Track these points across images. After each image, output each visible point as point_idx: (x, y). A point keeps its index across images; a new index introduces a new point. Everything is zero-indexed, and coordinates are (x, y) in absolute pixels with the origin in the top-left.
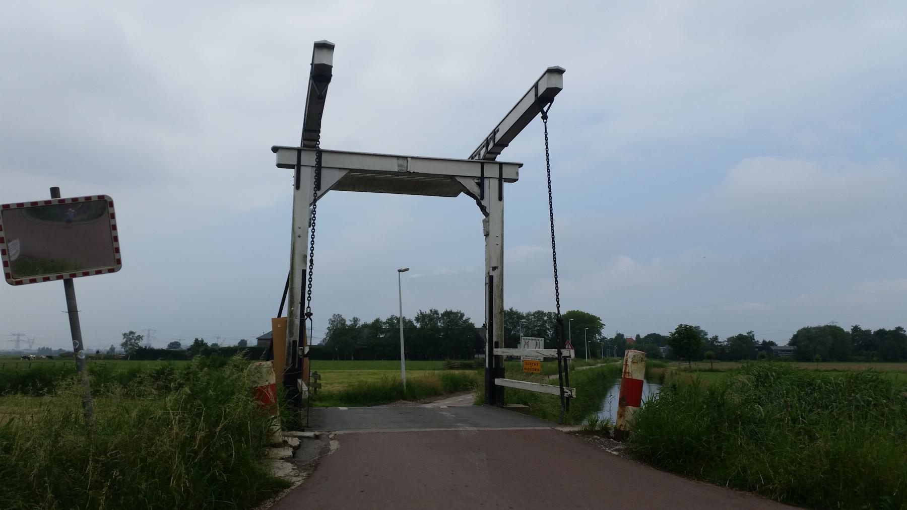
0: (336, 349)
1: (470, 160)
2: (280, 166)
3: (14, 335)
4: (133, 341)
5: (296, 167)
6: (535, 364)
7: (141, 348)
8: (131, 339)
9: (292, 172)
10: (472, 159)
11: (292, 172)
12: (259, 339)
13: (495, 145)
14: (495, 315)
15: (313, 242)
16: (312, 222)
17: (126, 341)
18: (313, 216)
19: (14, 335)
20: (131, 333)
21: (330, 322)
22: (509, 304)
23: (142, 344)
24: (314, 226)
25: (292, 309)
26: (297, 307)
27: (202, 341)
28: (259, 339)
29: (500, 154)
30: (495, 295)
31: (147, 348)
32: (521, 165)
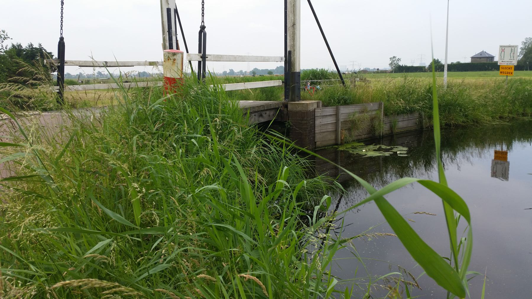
0: (528, 63)
3: (351, 62)
4: (395, 62)
6: (509, 68)
7: (400, 66)
8: (394, 61)
12: (472, 58)
14: (288, 29)
17: (392, 62)
19: (351, 62)
20: (394, 57)
21: (522, 44)
23: (401, 63)
25: (164, 36)
26: (167, 35)
27: (438, 60)
28: (472, 58)
30: (289, 11)
31: (403, 66)
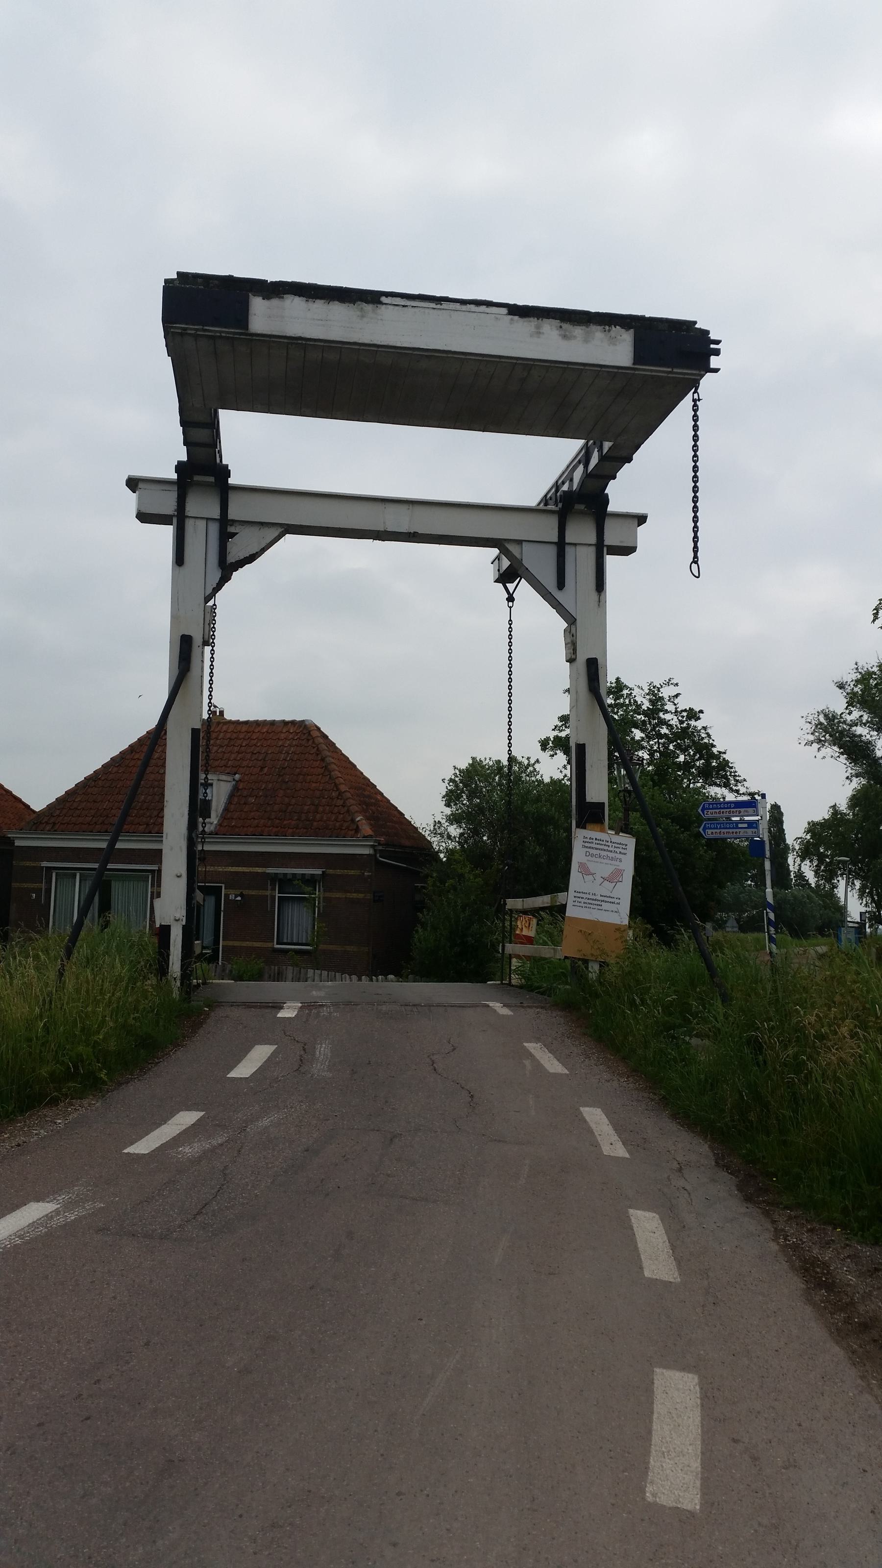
1: (542, 506)
2: (144, 517)
5: (175, 520)
9: (167, 532)
10: (546, 504)
11: (167, 532)
13: (602, 458)
15: (211, 674)
16: (212, 633)
18: (212, 633)
22: (589, 799)
24: (213, 647)
29: (629, 460)
32: (641, 519)
